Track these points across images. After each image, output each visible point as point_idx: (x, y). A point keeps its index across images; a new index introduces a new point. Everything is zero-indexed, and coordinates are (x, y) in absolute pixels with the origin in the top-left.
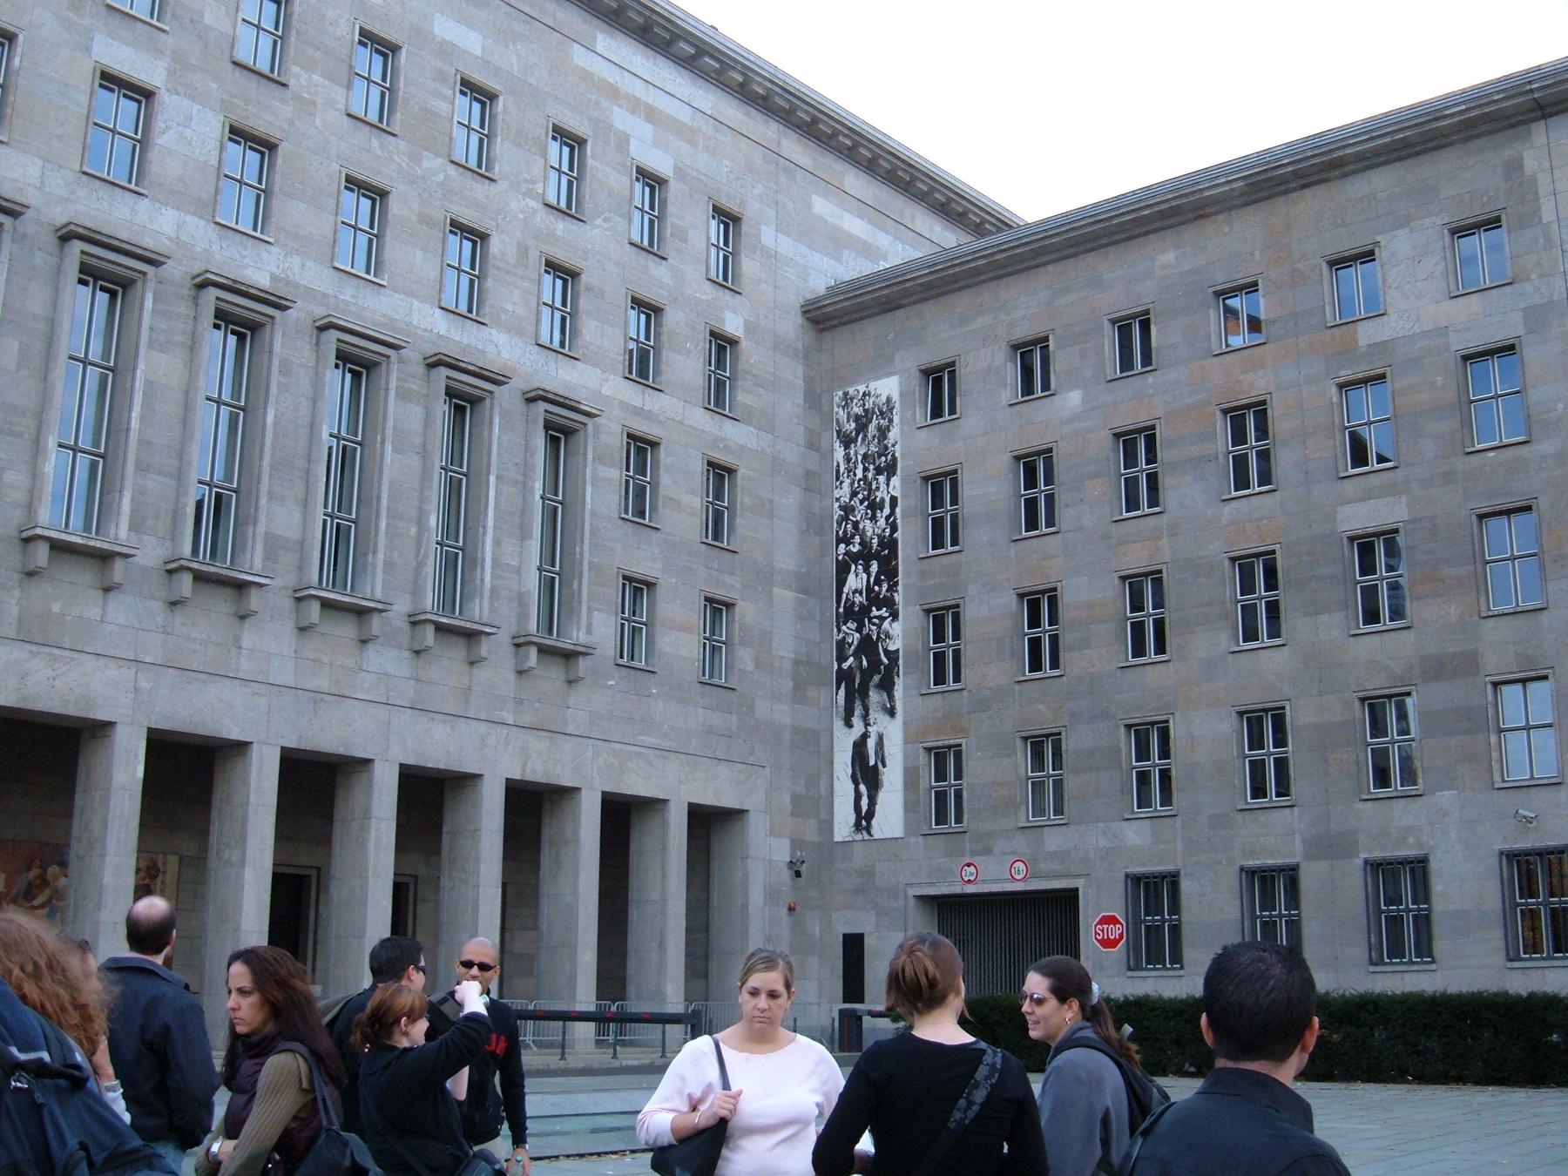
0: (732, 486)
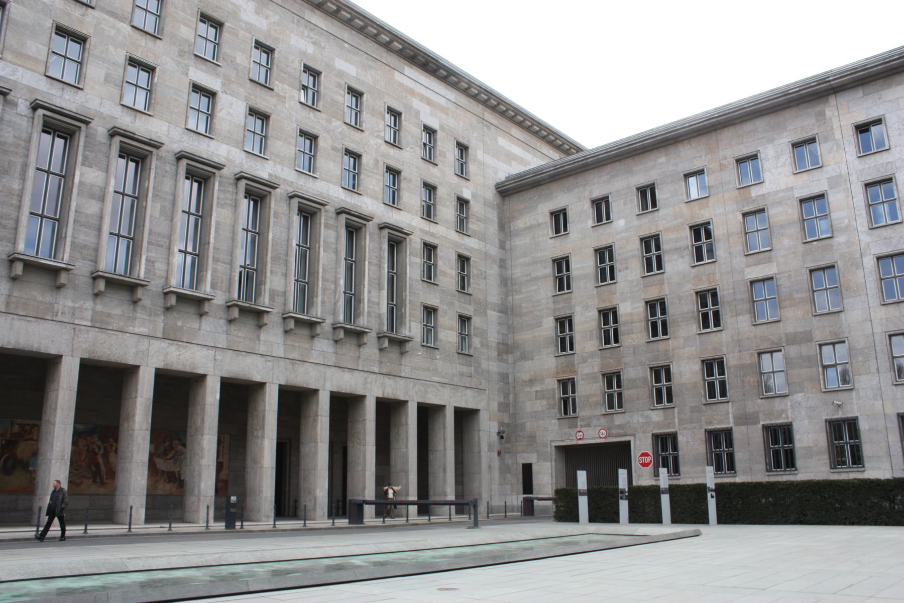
0: (469, 265)
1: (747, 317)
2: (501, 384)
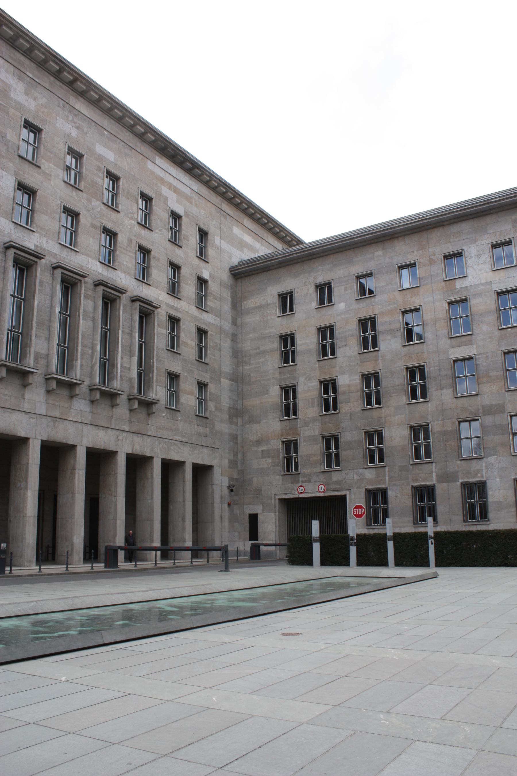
0: (206, 338)
1: (450, 390)
2: (231, 443)
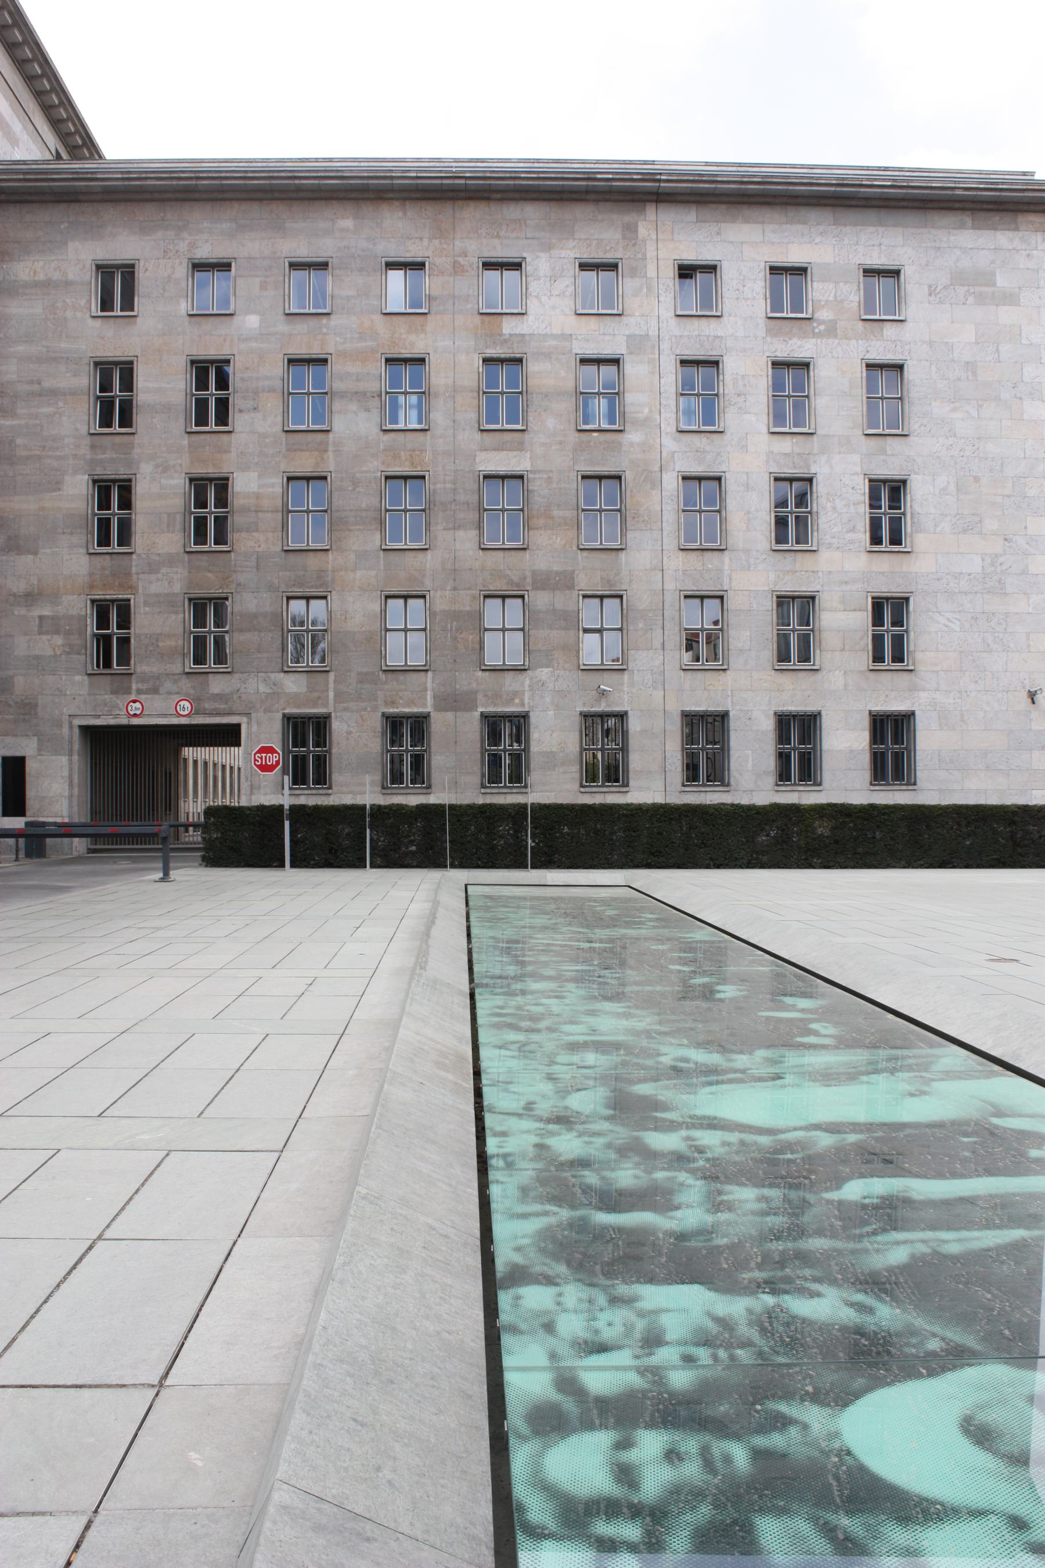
1: (473, 533)
